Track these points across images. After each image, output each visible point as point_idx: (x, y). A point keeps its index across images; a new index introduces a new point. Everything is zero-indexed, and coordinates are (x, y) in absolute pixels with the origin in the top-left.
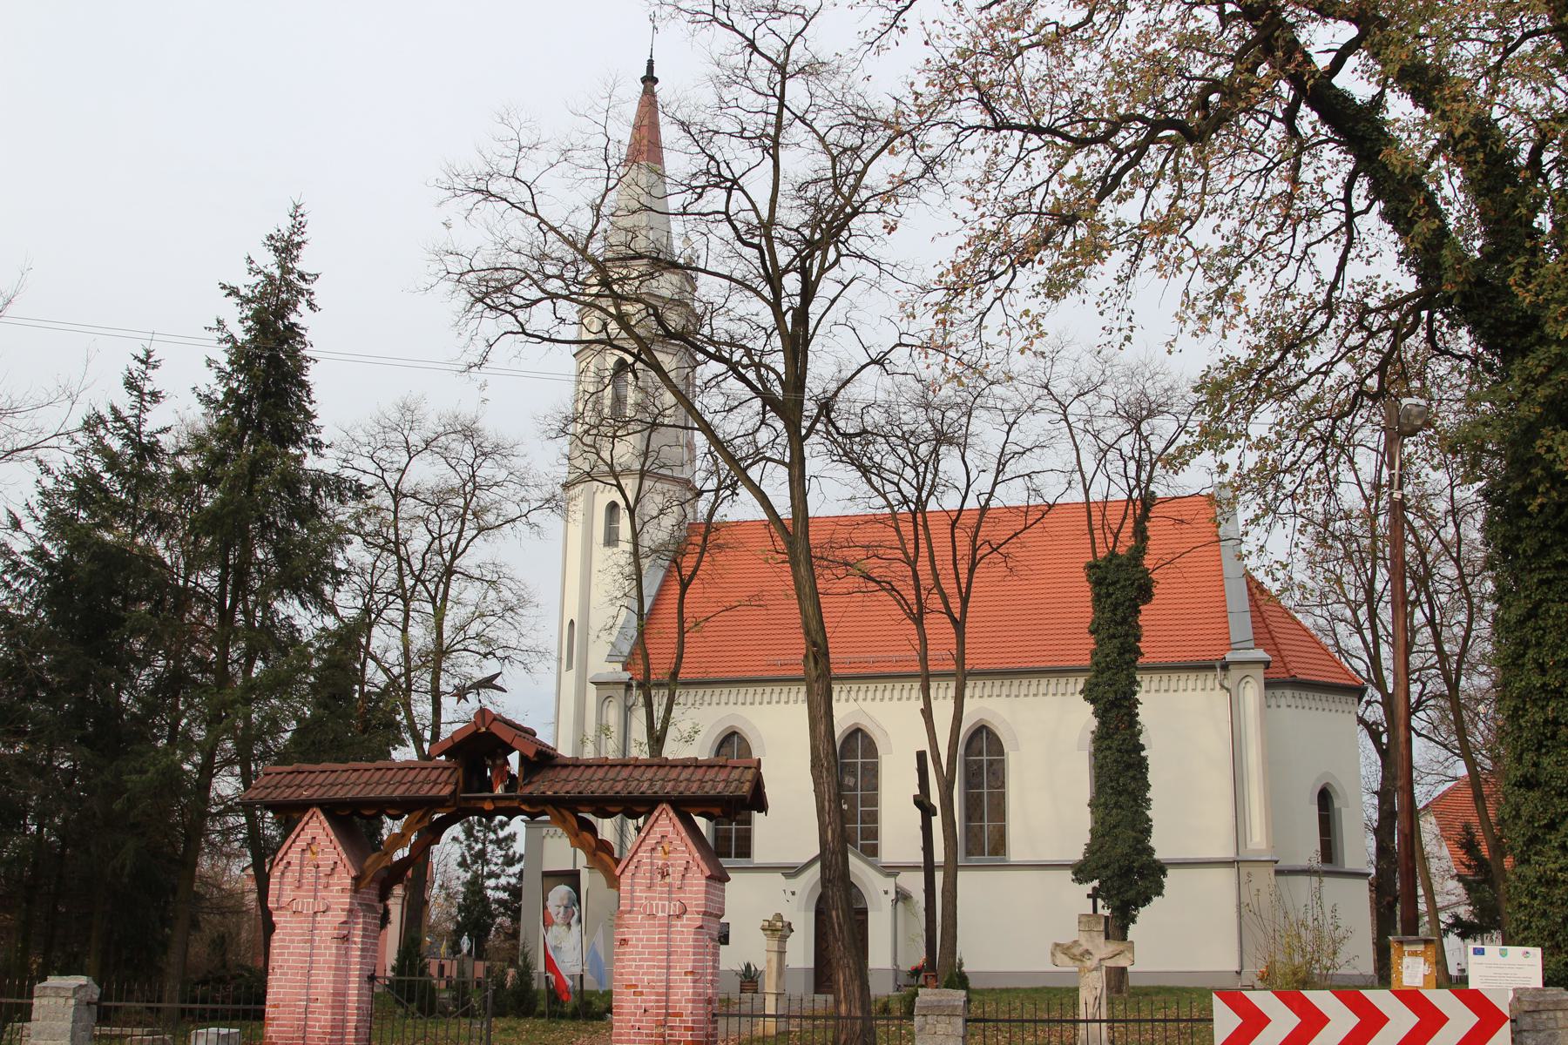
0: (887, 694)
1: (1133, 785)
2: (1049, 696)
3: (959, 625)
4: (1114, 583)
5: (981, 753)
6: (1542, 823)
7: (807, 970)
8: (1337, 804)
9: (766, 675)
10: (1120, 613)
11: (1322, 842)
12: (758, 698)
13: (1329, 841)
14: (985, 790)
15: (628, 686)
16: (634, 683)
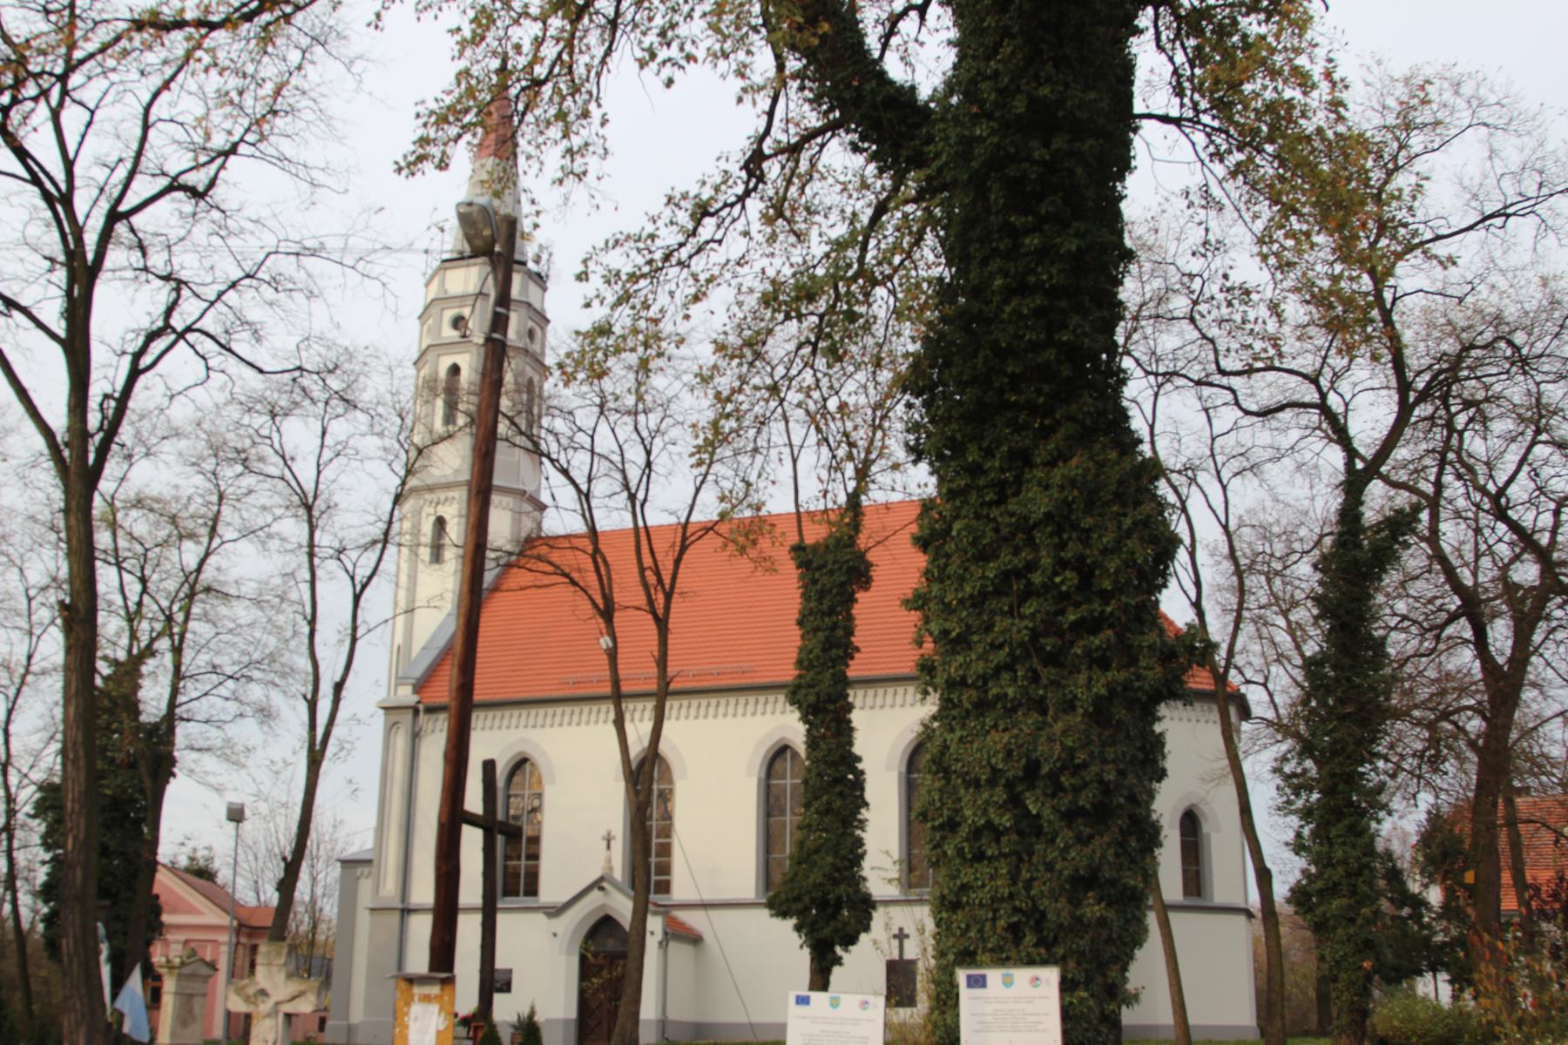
0: (683, 712)
1: (838, 803)
2: (887, 708)
3: (662, 623)
4: (820, 568)
5: (784, 777)
6: (937, 823)
7: (566, 1021)
8: (1206, 828)
9: (555, 694)
10: (826, 603)
11: (1185, 872)
12: (549, 720)
13: (1198, 873)
14: (788, 817)
15: (416, 711)
16: (421, 707)
